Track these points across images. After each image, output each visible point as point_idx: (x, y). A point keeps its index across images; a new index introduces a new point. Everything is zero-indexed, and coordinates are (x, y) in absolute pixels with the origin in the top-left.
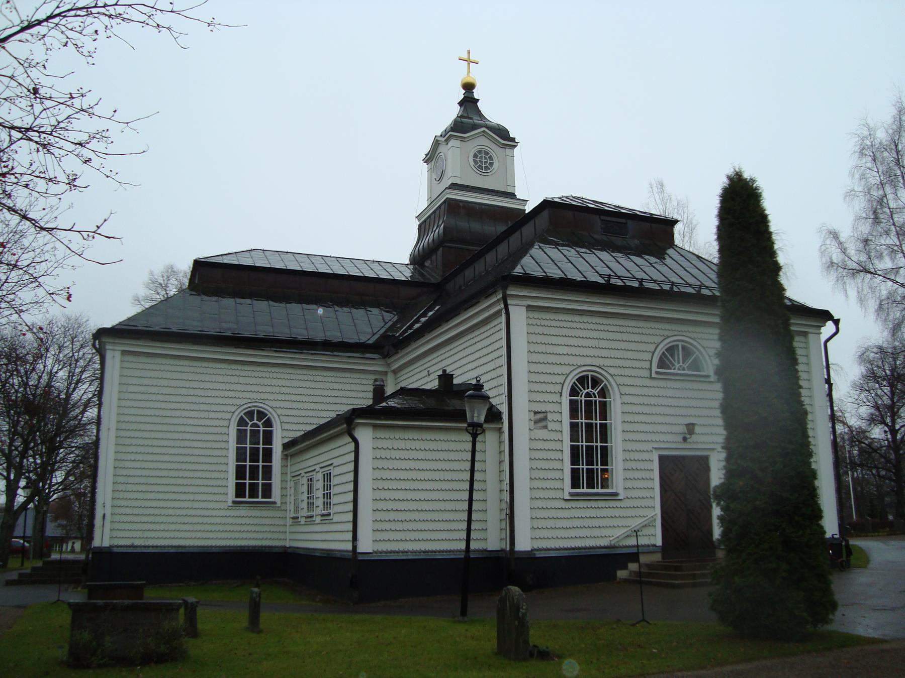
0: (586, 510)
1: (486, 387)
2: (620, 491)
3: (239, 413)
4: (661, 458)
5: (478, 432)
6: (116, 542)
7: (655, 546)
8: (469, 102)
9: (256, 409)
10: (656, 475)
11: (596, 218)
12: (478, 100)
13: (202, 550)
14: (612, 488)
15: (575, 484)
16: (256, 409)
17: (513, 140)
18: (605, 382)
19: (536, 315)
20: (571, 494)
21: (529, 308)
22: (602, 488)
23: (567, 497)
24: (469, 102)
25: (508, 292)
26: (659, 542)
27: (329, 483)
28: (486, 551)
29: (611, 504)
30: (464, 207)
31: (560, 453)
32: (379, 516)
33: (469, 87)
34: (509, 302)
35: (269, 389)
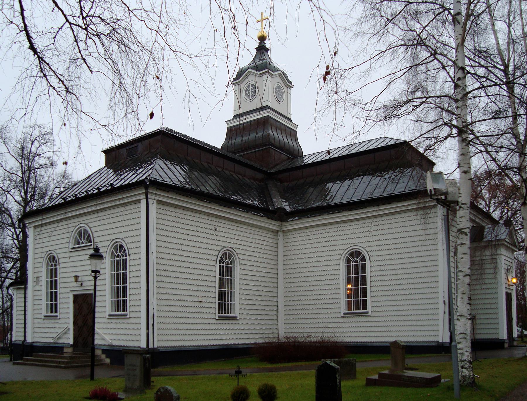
0: (228, 325)
1: (101, 251)
2: (238, 315)
3: (345, 254)
4: (76, 297)
5: (97, 276)
6: (36, 340)
7: (69, 344)
8: (262, 49)
9: (355, 250)
10: (71, 305)
11: (124, 151)
12: (256, 48)
13: (225, 347)
14: (231, 313)
15: (349, 308)
16: (355, 250)
17: (291, 83)
18: (363, 253)
19: (161, 206)
20: (219, 317)
21: (159, 202)
22: (117, 311)
23: (217, 318)
24: (262, 49)
25: (149, 191)
26: (71, 341)
27: (54, 302)
28: (140, 347)
29: (234, 322)
30: (251, 125)
31: (276, 293)
32: (287, 326)
33: (262, 39)
34: (149, 196)
35: (338, 238)
